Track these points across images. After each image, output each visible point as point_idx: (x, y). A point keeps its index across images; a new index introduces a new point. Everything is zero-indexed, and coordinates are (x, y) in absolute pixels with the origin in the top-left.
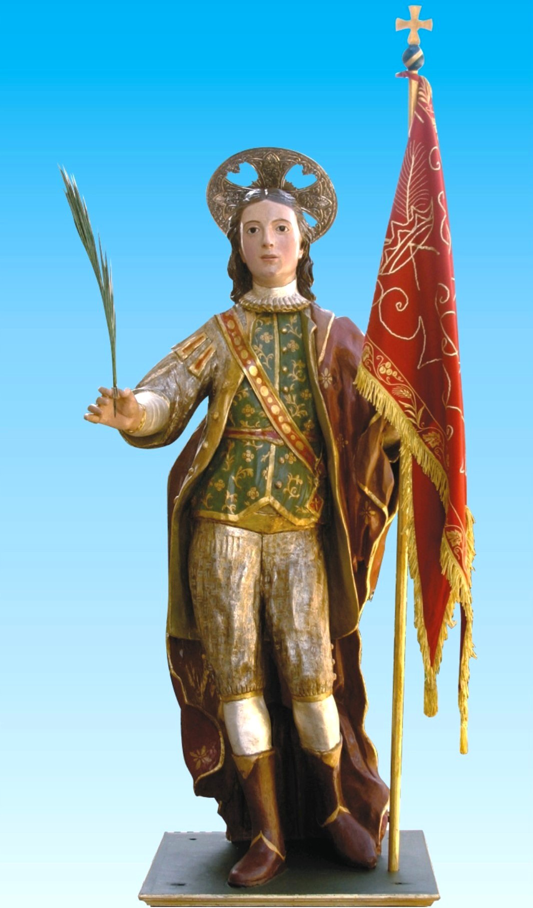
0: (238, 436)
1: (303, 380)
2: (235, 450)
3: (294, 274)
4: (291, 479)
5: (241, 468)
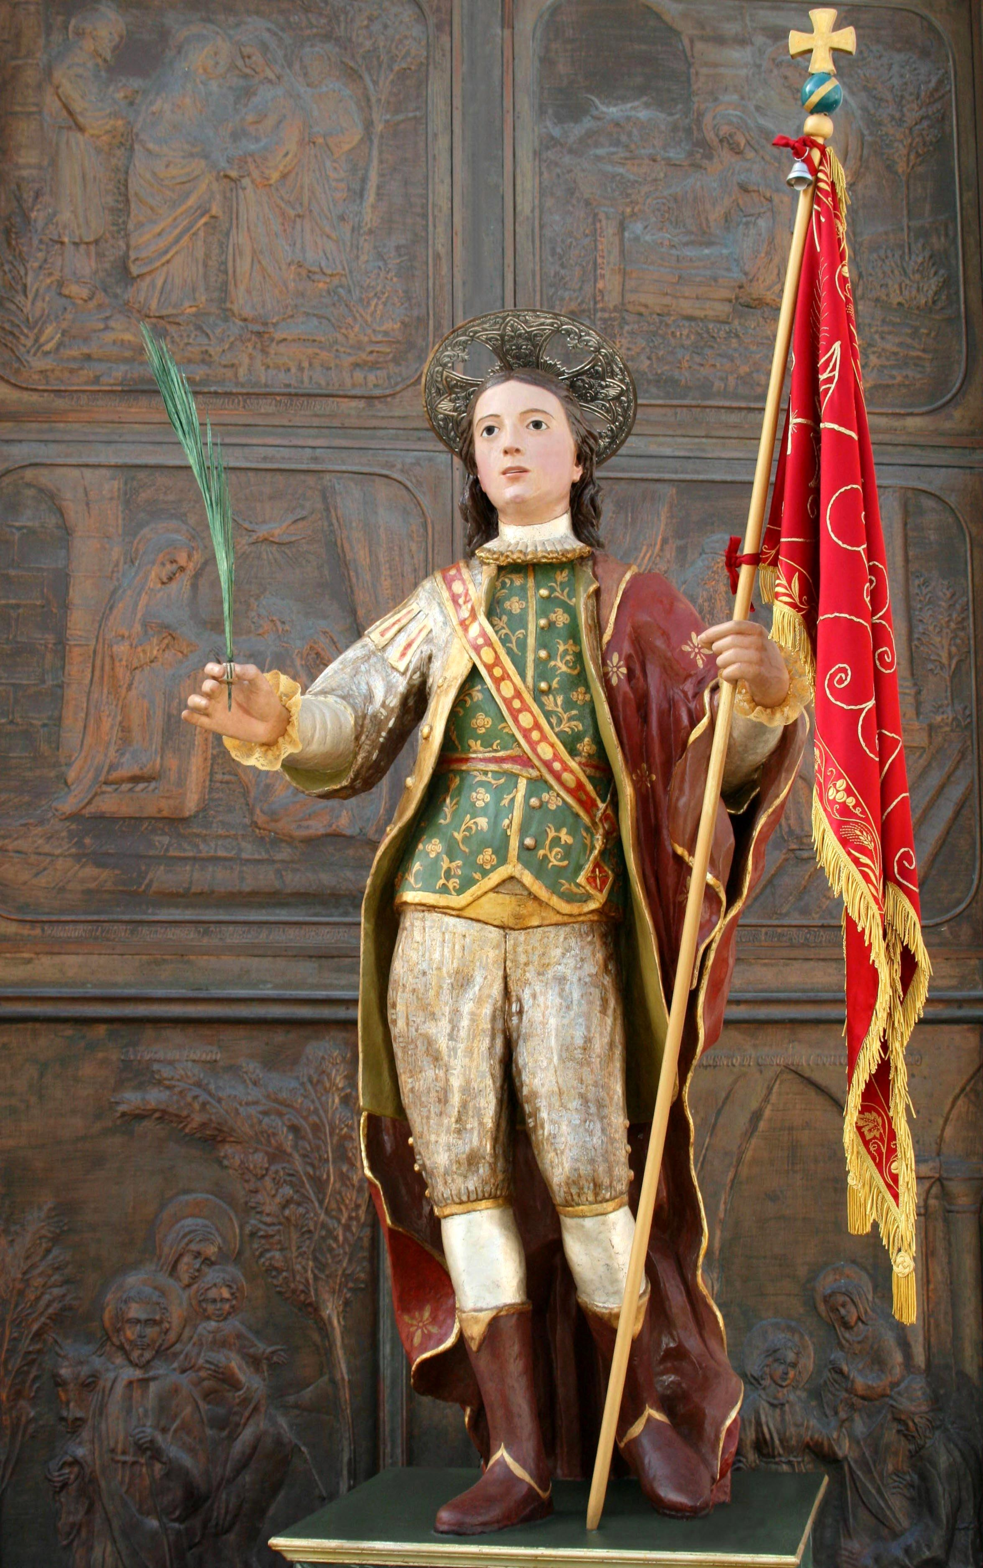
1: (576, 672)
2: (459, 790)
3: (565, 503)
4: (552, 834)
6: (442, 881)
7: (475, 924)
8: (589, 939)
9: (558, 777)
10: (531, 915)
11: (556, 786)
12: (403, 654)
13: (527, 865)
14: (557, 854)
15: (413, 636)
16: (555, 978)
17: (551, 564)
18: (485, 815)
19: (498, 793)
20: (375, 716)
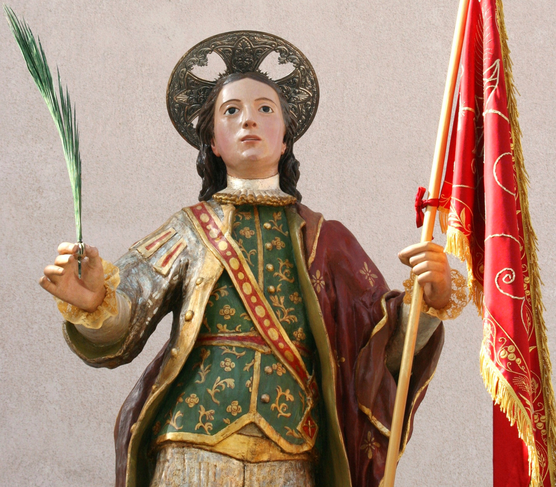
0: (214, 343)
1: (292, 281)
2: (211, 360)
5: (219, 378)
6: (199, 425)
7: (223, 457)
8: (302, 473)
9: (282, 352)
10: (262, 452)
12: (166, 262)
14: (283, 408)
15: (172, 250)
17: (272, 206)
18: (232, 377)
20: (144, 305)
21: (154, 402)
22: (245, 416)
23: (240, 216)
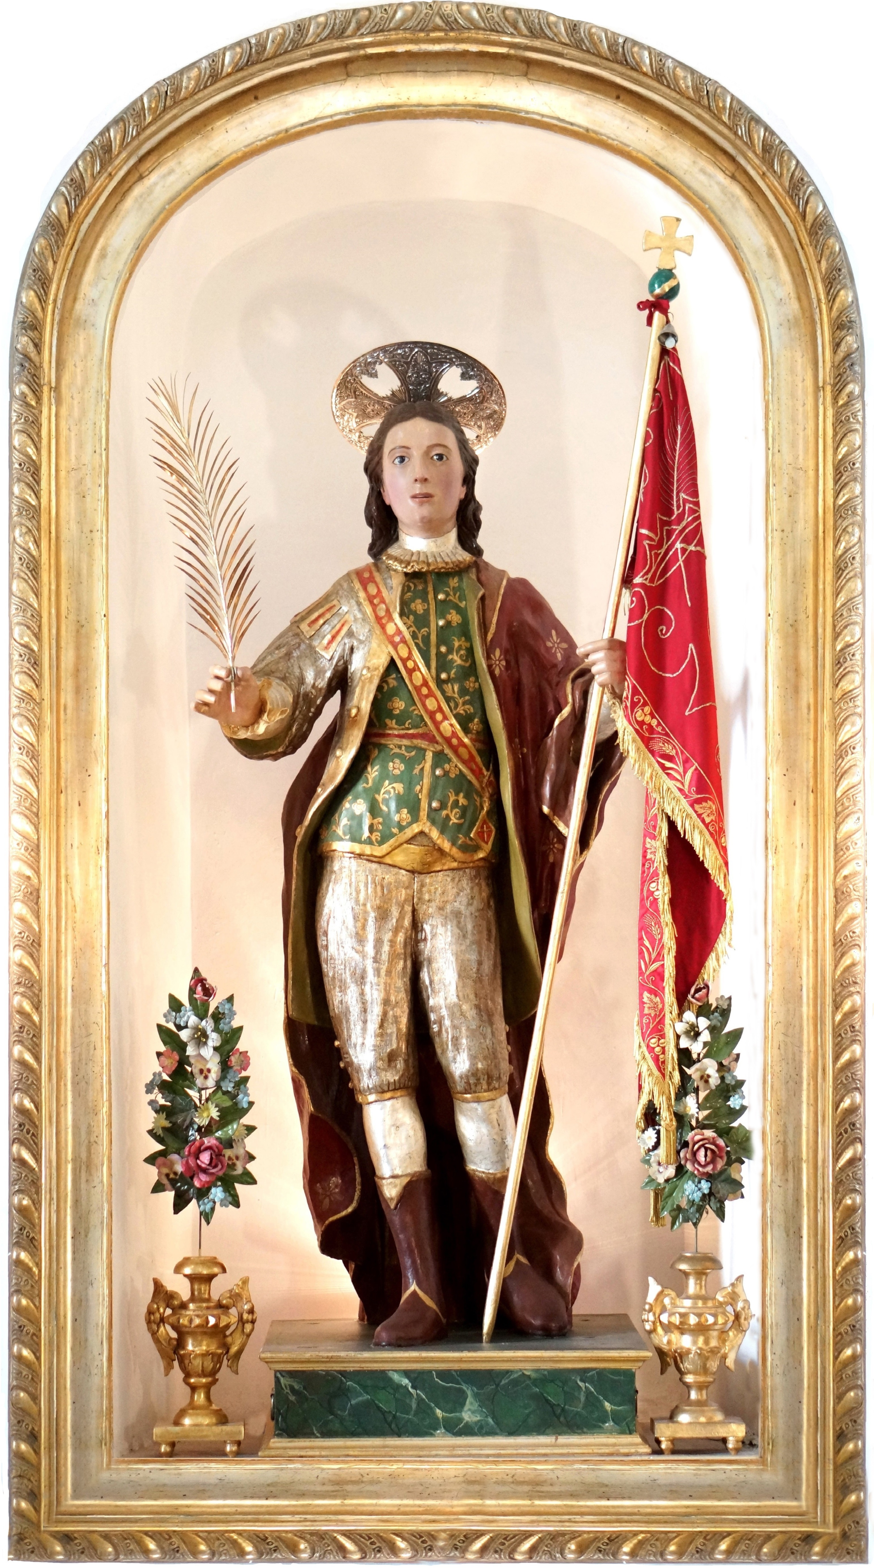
0: (383, 741)
1: (467, 665)
3: (454, 520)
7: (392, 869)
9: (455, 749)
10: (435, 862)
11: (455, 759)
13: (433, 822)
16: (452, 912)
18: (401, 782)
19: (410, 763)
21: (305, 867)
22: (415, 825)
23: (412, 585)
